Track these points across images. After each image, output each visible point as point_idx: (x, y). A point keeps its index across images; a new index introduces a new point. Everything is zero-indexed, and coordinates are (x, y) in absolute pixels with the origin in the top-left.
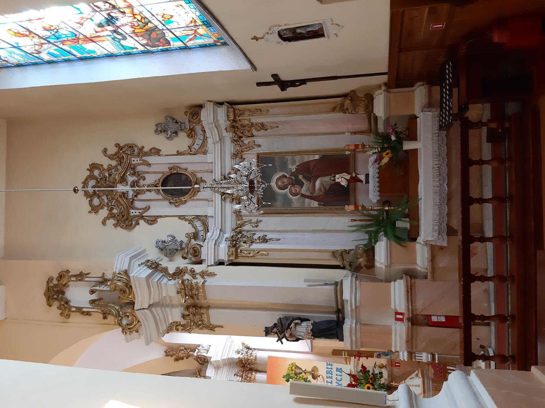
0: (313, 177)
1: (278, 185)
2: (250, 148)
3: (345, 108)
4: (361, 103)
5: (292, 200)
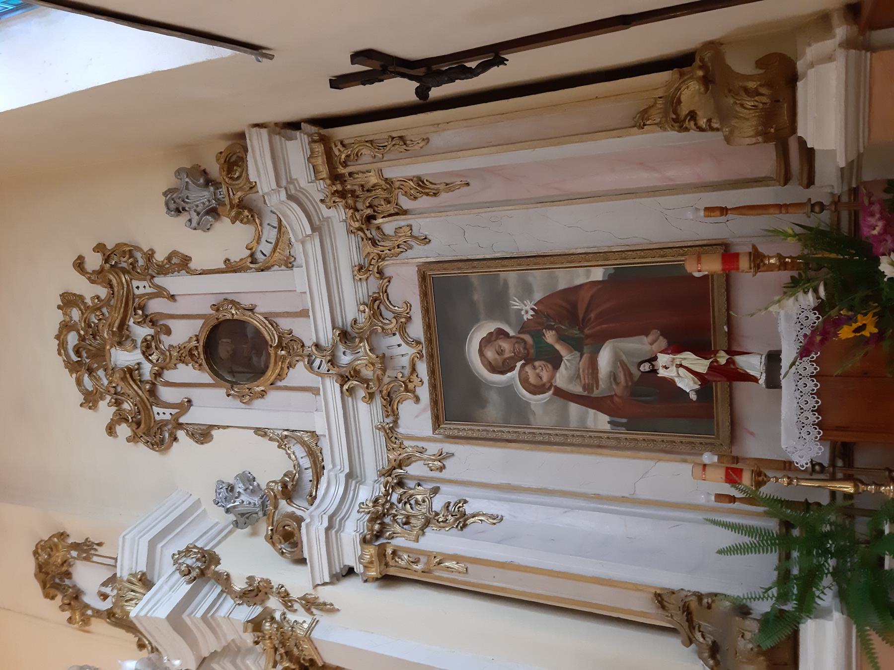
0: (588, 336)
1: (487, 360)
2: (401, 248)
3: (684, 110)
4: (742, 105)
5: (528, 404)
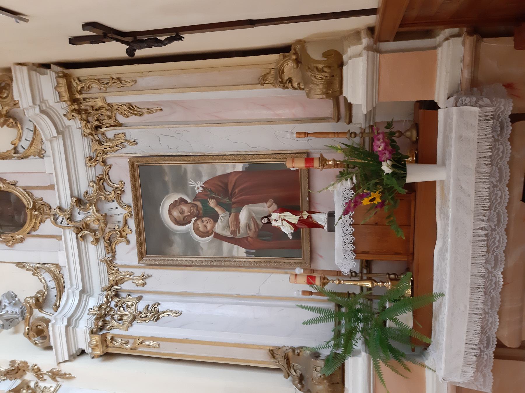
0: (234, 203)
1: (174, 217)
2: (118, 147)
3: (286, 78)
5: (199, 243)
